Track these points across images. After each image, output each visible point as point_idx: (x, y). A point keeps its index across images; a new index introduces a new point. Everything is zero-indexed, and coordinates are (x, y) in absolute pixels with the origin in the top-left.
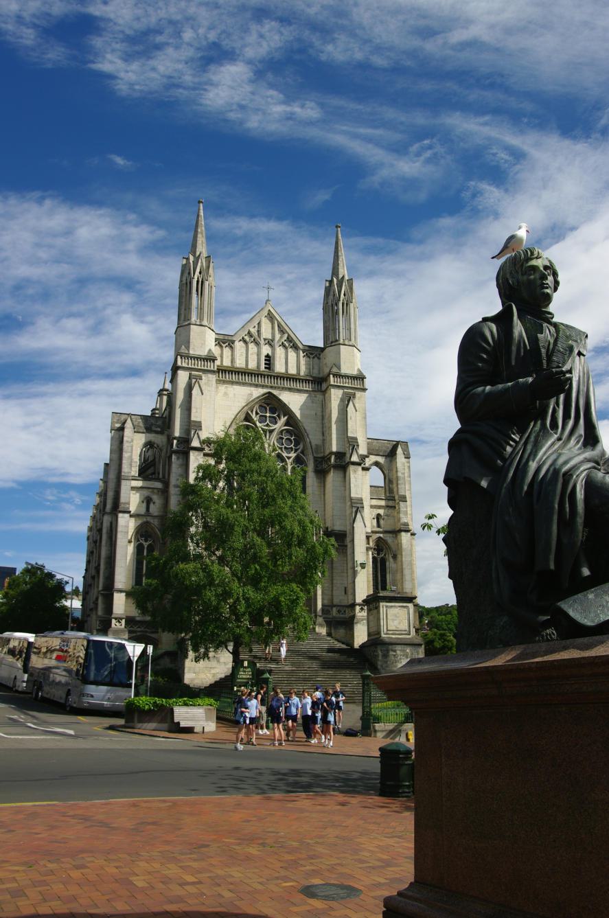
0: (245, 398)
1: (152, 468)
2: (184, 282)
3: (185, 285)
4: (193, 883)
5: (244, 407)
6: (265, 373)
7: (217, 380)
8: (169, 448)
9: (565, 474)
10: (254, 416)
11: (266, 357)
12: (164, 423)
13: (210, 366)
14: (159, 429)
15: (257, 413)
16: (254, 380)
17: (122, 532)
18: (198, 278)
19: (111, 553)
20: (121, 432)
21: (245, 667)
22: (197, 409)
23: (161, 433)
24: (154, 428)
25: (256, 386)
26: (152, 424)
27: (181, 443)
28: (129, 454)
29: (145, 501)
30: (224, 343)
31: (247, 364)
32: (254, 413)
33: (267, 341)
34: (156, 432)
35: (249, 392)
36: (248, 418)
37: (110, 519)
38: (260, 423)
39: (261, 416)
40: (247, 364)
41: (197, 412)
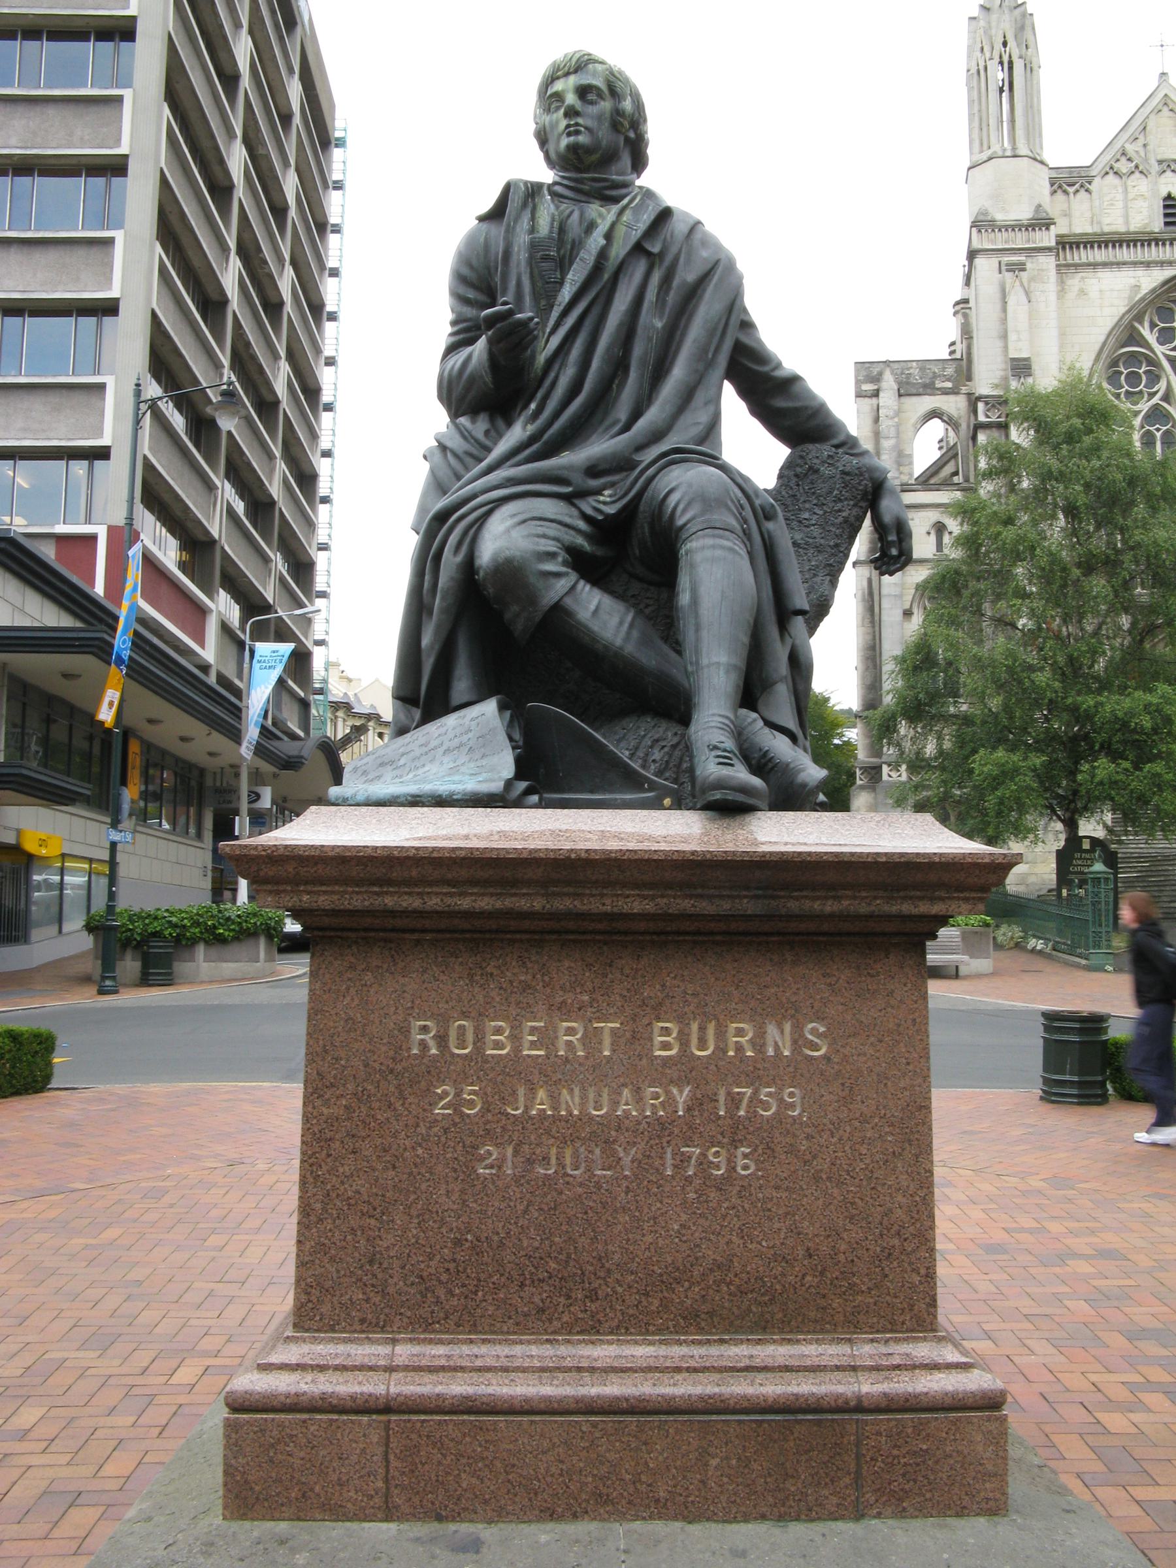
0: (1126, 294)
1: (952, 463)
2: (974, 71)
3: (976, 76)
4: (1031, 1231)
5: (1124, 315)
6: (1166, 236)
7: (1057, 266)
8: (972, 418)
9: (274, 724)
10: (1145, 331)
11: (1165, 199)
12: (958, 371)
13: (1047, 239)
14: (949, 385)
15: (1153, 325)
16: (1140, 254)
17: (889, 595)
18: (1001, 57)
19: (874, 638)
20: (874, 400)
21: (1086, 851)
22: (1018, 332)
23: (954, 392)
24: (939, 385)
25: (1148, 265)
26: (935, 376)
27: (993, 406)
28: (892, 442)
29: (933, 532)
30: (1071, 185)
31: (1127, 223)
32: (1147, 324)
33: (1165, 165)
34: (945, 392)
35: (1133, 281)
36: (1133, 337)
37: (868, 575)
38: (1161, 344)
39: (1162, 330)
40: (1127, 223)
41: (1019, 340)
